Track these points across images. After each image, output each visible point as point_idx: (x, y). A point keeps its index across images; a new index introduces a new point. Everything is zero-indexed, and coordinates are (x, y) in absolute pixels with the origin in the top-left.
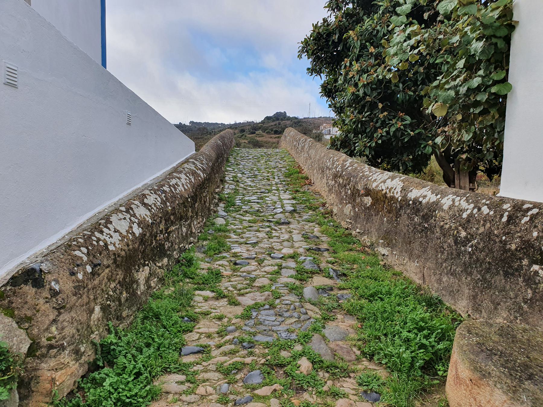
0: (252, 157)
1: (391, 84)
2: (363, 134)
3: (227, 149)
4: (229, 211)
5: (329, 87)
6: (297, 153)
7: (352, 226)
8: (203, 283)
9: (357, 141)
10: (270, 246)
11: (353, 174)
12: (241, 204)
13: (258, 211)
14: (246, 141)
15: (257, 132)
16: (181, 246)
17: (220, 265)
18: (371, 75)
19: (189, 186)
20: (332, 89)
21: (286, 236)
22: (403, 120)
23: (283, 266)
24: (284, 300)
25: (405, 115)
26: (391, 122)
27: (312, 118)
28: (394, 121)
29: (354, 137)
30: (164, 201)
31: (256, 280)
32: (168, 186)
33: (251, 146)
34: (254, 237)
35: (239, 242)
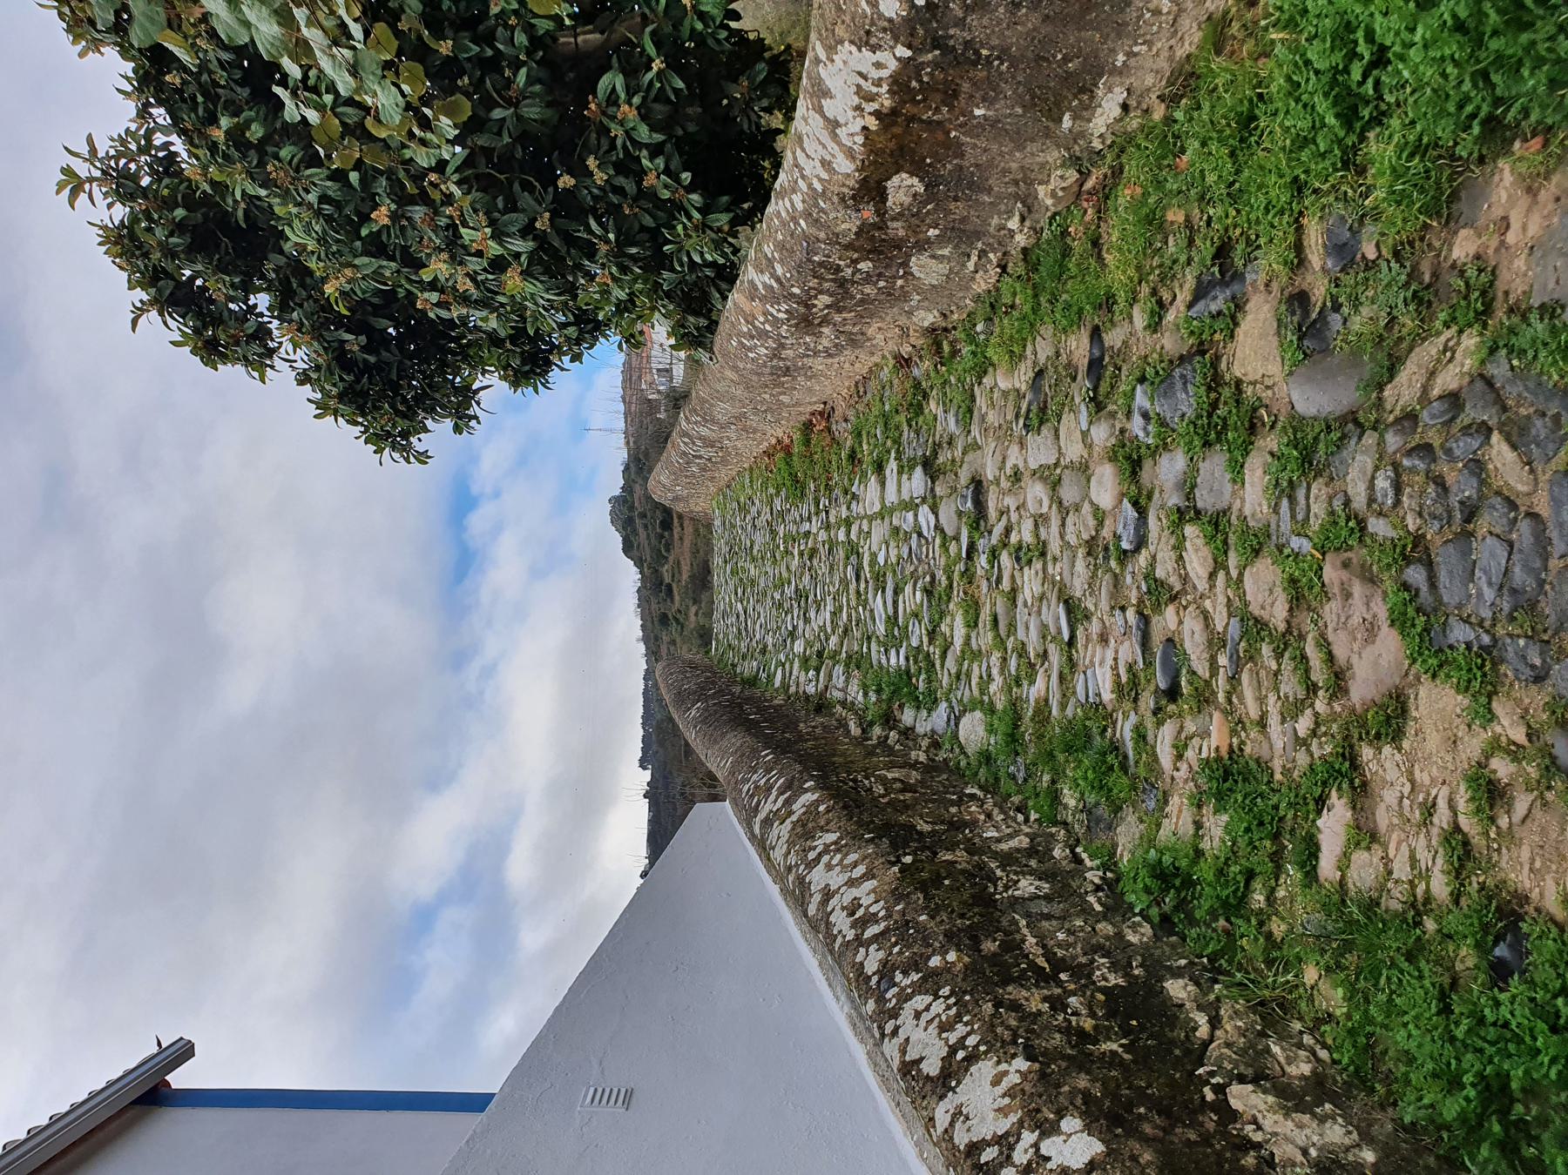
0: (739, 604)
1: (494, 149)
2: (661, 241)
3: (713, 683)
4: (931, 692)
5: (516, 362)
6: (724, 462)
7: (994, 251)
8: (1276, 837)
9: (685, 259)
10: (1081, 552)
11: (800, 255)
12: (902, 651)
13: (928, 592)
14: (693, 609)
15: (667, 580)
16: (1098, 908)
17: (1180, 757)
18: (462, 215)
19: (853, 857)
20: (522, 353)
21: (1036, 492)
22: (612, 99)
23: (1183, 504)
24: (1371, 500)
25: (595, 96)
26: (619, 142)
27: (626, 422)
28: (616, 131)
29: (673, 270)
30: (924, 979)
31: (1257, 612)
32: (862, 950)
33: (704, 597)
34: (1039, 612)
35: (1066, 671)
